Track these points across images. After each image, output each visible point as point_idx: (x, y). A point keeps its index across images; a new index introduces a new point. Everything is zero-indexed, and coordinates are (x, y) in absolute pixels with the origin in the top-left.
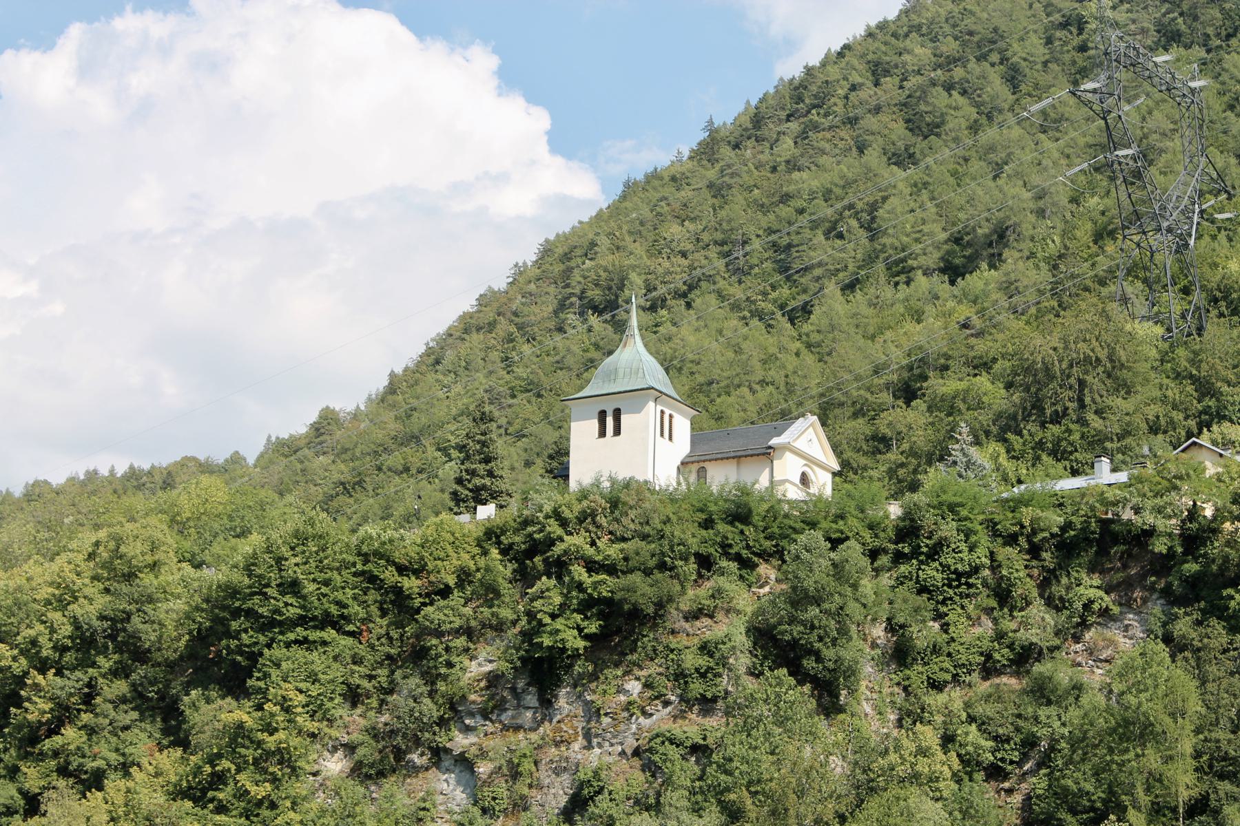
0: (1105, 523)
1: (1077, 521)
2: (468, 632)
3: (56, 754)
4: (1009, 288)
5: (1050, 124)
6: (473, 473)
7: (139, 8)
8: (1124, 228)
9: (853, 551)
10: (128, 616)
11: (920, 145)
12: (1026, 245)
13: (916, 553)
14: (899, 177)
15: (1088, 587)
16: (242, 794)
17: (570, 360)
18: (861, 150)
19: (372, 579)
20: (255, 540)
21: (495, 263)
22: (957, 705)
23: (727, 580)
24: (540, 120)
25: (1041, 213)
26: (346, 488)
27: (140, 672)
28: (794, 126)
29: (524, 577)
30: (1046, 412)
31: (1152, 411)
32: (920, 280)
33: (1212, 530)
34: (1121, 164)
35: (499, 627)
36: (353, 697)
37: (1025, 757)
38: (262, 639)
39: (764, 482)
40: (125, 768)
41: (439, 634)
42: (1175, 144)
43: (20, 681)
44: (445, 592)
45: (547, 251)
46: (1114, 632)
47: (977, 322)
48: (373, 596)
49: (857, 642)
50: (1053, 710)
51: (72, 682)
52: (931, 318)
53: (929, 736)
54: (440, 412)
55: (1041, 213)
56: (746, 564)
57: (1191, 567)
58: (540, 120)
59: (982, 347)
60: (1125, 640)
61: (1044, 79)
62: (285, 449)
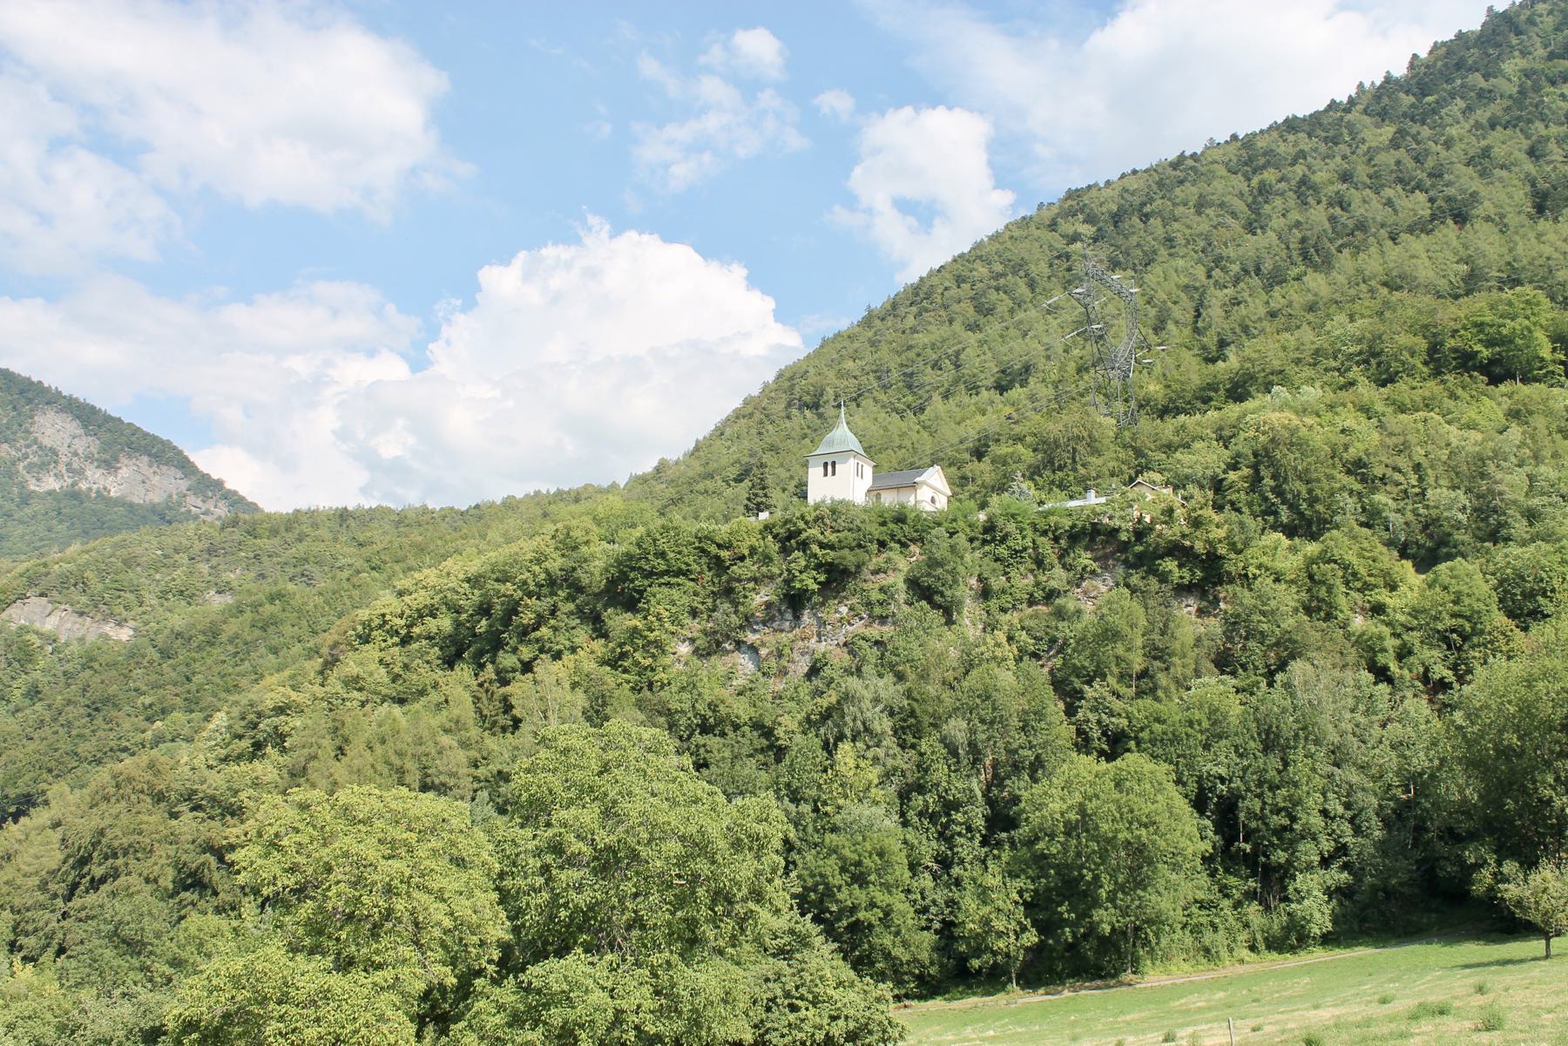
0: (1094, 525)
1: (1080, 524)
2: (755, 580)
3: (537, 641)
4: (1032, 398)
5: (1053, 310)
6: (756, 495)
7: (556, 243)
8: (1094, 365)
9: (961, 539)
10: (574, 569)
11: (982, 320)
12: (1041, 375)
13: (993, 540)
14: (972, 338)
15: (1085, 559)
16: (637, 663)
17: (793, 434)
18: (951, 322)
19: (703, 551)
20: (640, 531)
21: (754, 381)
22: (1016, 621)
23: (894, 553)
24: (770, 304)
25: (1048, 358)
26: (674, 502)
27: (581, 599)
28: (914, 309)
29: (785, 551)
30: (1056, 464)
31: (1111, 465)
32: (984, 393)
33: (1150, 529)
34: (1088, 328)
35: (772, 578)
36: (694, 613)
37: (1050, 648)
38: (646, 583)
39: (912, 502)
40: (573, 650)
41: (739, 580)
42: (1122, 322)
43: (518, 603)
44: (742, 558)
45: (780, 375)
46: (1098, 583)
47: (1015, 415)
48: (704, 560)
49: (962, 587)
50: (1066, 624)
51: (546, 603)
52: (989, 414)
53: (1001, 636)
54: (724, 461)
55: (1048, 358)
56: (904, 545)
57: (1139, 548)
58: (770, 304)
59: (1018, 429)
60: (1101, 586)
61: (1048, 286)
62: (643, 480)
